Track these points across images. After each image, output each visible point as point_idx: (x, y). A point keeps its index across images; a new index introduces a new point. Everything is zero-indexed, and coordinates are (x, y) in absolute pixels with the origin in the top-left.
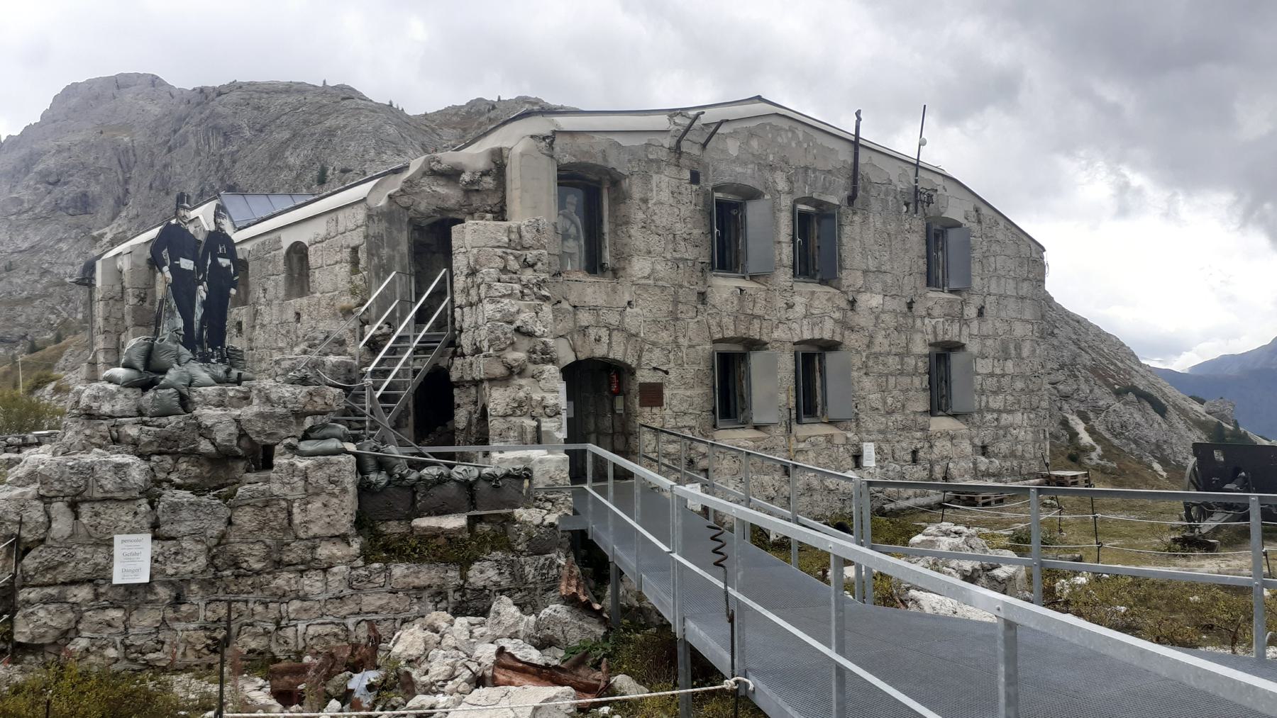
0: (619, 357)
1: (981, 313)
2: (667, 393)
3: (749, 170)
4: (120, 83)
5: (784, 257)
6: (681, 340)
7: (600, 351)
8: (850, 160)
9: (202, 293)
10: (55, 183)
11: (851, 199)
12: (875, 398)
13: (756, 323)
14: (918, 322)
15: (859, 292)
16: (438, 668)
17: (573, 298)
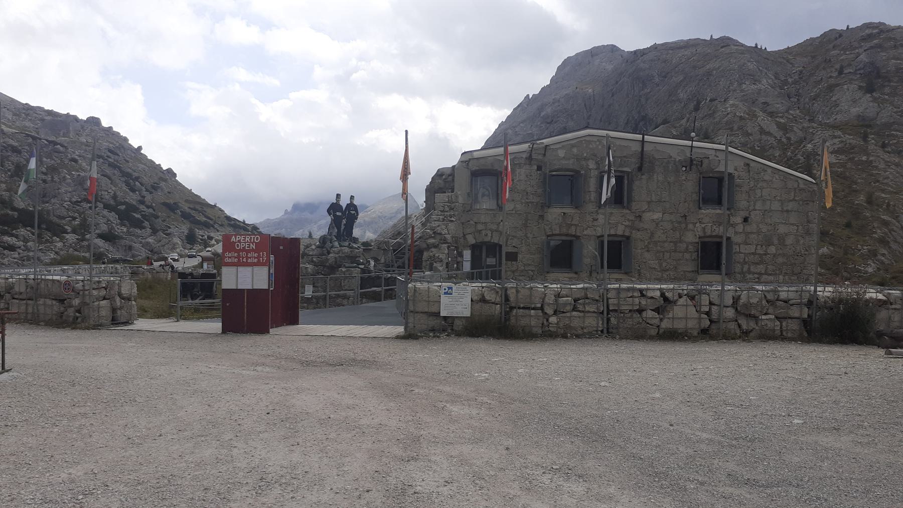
0: (496, 242)
1: (746, 220)
2: (520, 257)
3: (571, 162)
4: (594, 53)
5: (592, 198)
6: (529, 235)
7: (487, 239)
8: (640, 150)
9: (344, 221)
10: (550, 123)
11: (640, 169)
12: (654, 263)
13: (573, 228)
14: (690, 226)
15: (644, 212)
16: (123, 242)
17: (475, 220)
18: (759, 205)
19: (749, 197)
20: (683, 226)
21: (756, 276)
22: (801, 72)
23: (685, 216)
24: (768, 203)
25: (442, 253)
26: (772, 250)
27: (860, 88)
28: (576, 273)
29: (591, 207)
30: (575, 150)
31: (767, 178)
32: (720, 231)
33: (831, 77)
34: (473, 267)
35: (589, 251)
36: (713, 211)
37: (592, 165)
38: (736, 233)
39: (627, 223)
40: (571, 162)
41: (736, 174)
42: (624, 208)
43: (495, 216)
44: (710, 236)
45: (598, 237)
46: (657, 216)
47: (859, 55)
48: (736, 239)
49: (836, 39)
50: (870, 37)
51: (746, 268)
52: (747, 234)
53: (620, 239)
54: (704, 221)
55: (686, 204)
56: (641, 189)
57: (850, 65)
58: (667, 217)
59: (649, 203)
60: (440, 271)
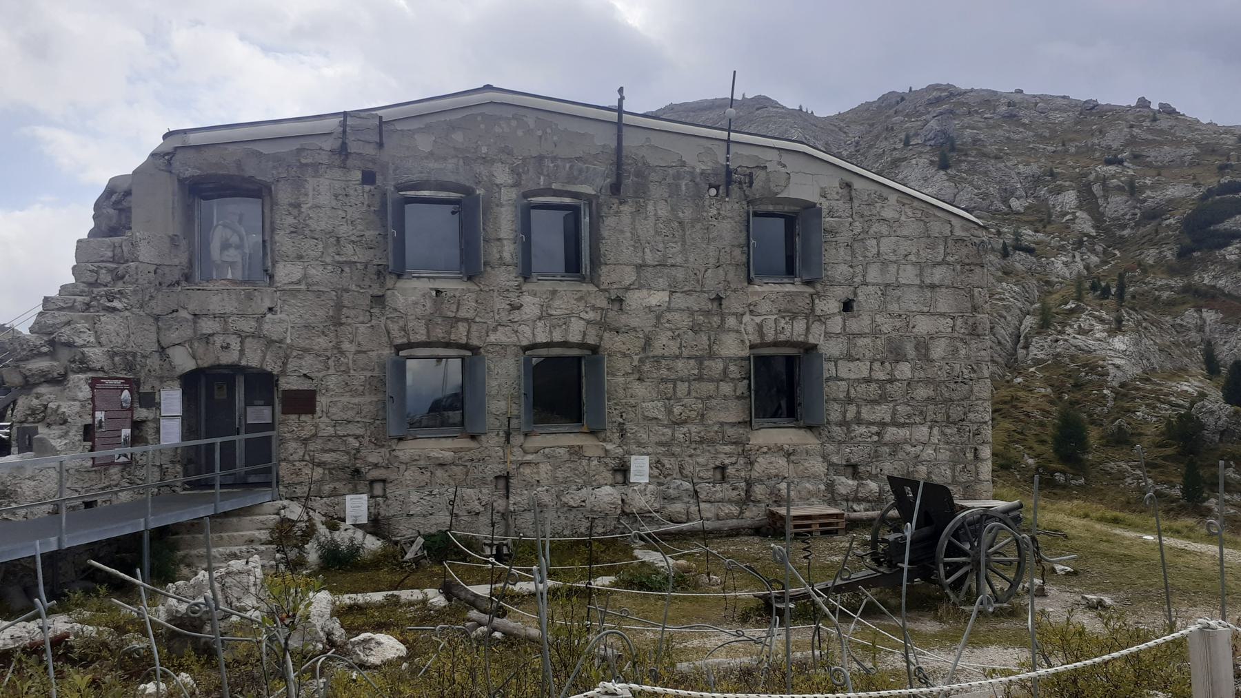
1: (847, 306)
2: (322, 401)
3: (450, 164)
6: (346, 346)
8: (614, 145)
11: (616, 189)
12: (655, 408)
13: (462, 328)
14: (731, 322)
15: (627, 289)
17: (192, 307)
18: (873, 274)
19: (853, 254)
20: (716, 320)
21: (874, 429)
22: (858, 143)
23: (719, 299)
24: (893, 268)
25: (73, 400)
26: (904, 370)
27: (932, 163)
28: (473, 437)
29: (505, 277)
30: (458, 137)
31: (888, 213)
32: (797, 330)
33: (895, 149)
34: (189, 431)
35: (503, 382)
36: (778, 288)
37: (502, 175)
38: (828, 335)
39: (591, 315)
40: (450, 164)
41: (825, 205)
42: (583, 279)
43: (249, 297)
44: (776, 344)
45: (526, 349)
46: (658, 298)
47: (927, 122)
48: (831, 348)
49: (898, 103)
50: (938, 101)
51: (851, 412)
52: (852, 337)
53: (575, 352)
54: (759, 309)
55: (721, 271)
56: (623, 235)
57: (917, 135)
58: (680, 301)
59: (639, 267)
60: (54, 451)
